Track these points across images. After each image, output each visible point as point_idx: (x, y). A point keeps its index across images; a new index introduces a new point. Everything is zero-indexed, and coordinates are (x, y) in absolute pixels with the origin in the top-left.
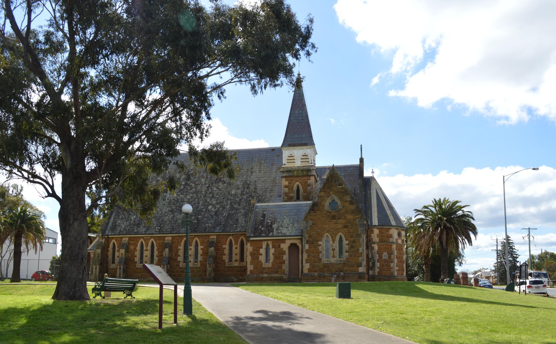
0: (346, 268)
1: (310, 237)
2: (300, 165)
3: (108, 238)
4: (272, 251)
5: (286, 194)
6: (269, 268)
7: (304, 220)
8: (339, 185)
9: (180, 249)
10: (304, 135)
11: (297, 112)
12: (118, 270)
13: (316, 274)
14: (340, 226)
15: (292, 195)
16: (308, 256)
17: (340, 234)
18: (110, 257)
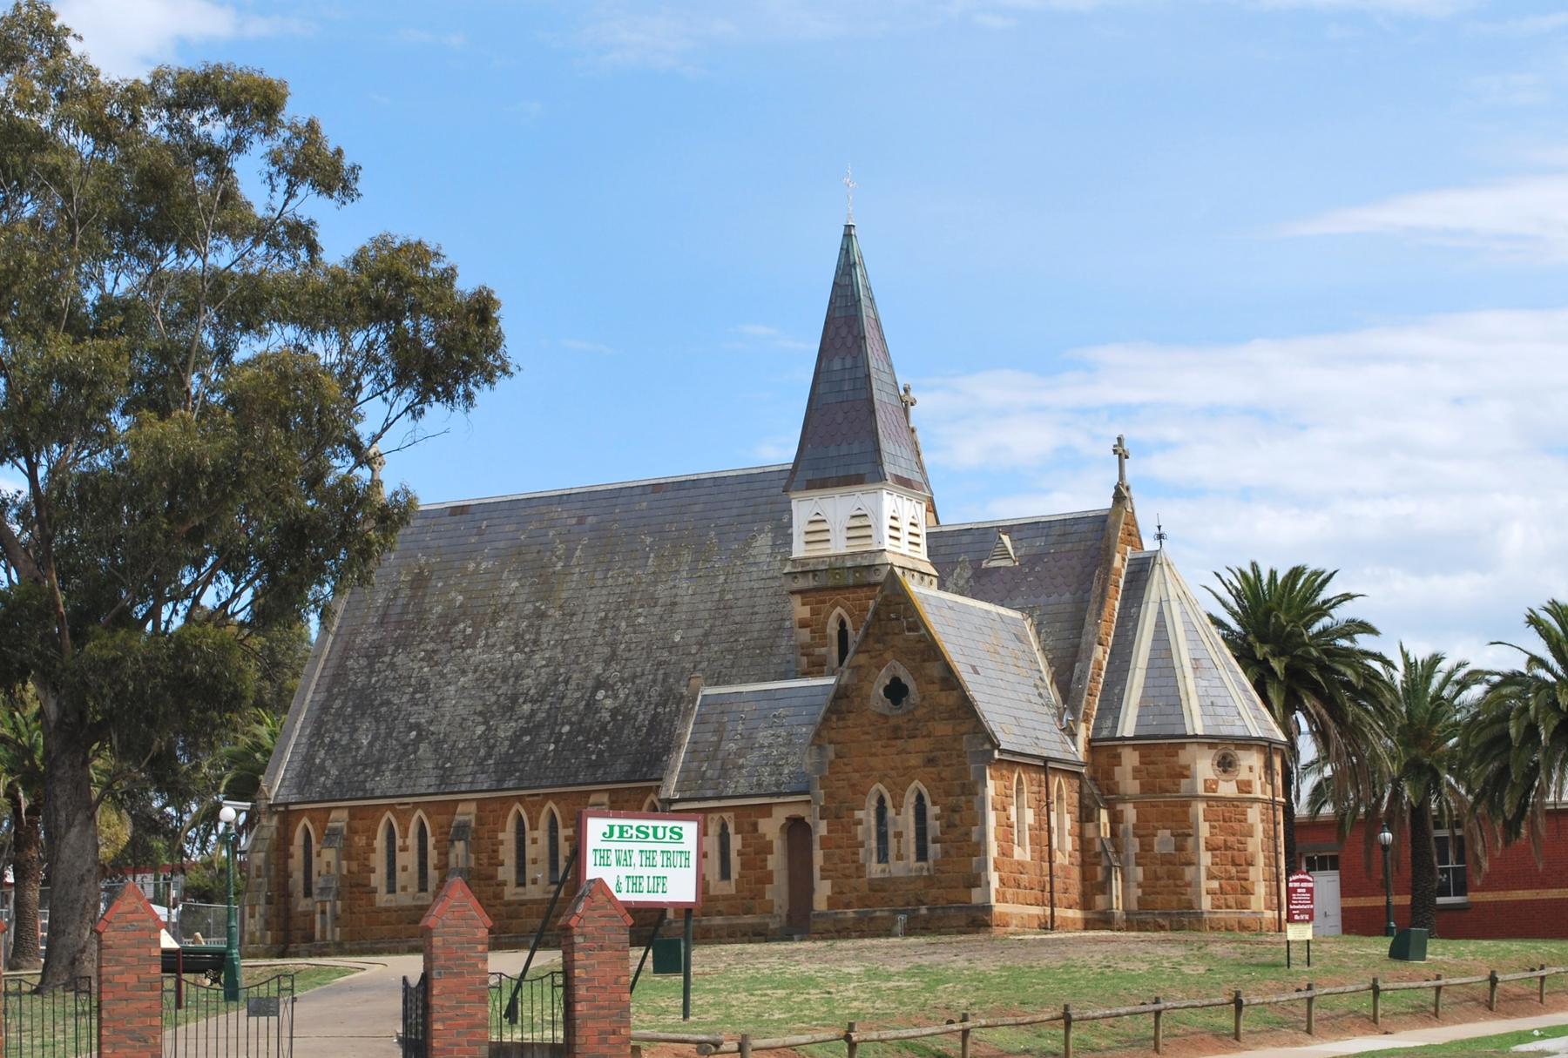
0: (934, 892)
1: (830, 796)
2: (844, 551)
3: (288, 812)
4: (736, 842)
5: (805, 650)
6: (726, 898)
7: (812, 744)
8: (910, 630)
9: (502, 843)
10: (856, 448)
11: (837, 365)
12: (318, 917)
13: (850, 913)
14: (914, 760)
15: (823, 650)
16: (827, 858)
17: (916, 784)
18: (298, 876)
